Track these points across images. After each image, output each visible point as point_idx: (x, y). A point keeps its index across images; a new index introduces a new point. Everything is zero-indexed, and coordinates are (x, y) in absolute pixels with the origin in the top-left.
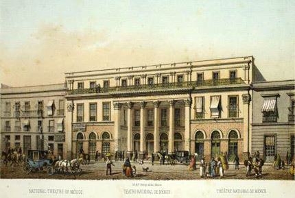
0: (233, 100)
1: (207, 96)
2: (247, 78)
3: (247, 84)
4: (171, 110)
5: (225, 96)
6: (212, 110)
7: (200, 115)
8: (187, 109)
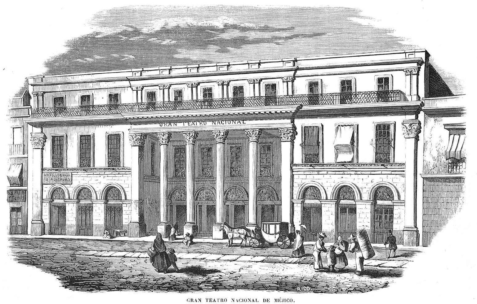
0: (383, 134)
1: (329, 124)
2: (414, 92)
3: (413, 101)
4: (252, 148)
5: (367, 126)
6: (338, 149)
7: (312, 158)
8: (286, 147)
